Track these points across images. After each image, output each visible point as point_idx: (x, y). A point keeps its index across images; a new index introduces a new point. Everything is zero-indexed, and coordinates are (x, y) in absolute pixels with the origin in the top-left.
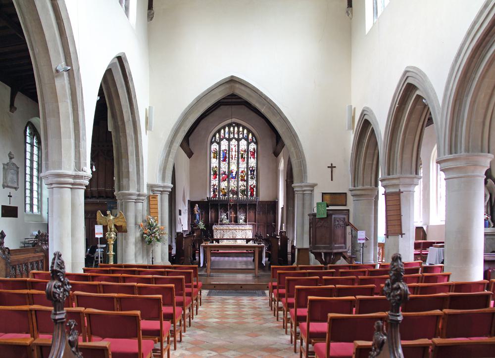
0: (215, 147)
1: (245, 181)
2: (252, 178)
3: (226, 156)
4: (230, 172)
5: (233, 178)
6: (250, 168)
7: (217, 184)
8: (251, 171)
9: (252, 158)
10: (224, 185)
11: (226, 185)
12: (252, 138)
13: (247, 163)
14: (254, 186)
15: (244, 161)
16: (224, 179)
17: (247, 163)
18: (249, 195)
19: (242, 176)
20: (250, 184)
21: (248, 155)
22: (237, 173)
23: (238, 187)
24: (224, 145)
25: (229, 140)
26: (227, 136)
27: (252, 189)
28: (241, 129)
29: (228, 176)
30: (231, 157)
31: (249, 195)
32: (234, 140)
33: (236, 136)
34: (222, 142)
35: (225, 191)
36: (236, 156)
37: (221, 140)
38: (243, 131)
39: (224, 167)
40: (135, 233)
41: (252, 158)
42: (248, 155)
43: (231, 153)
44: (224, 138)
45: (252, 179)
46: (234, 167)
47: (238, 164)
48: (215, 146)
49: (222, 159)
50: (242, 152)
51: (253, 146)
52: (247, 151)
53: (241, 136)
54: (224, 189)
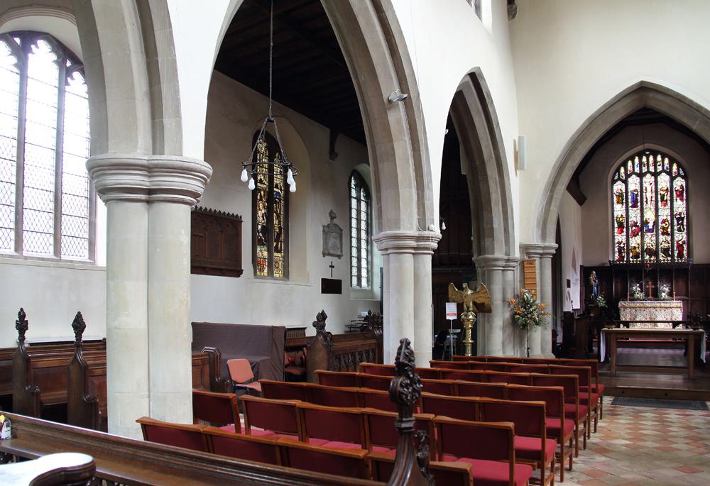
0: (619, 187)
1: (668, 234)
2: (679, 230)
6: (676, 215)
10: (635, 242)
11: (639, 242)
14: (684, 243)
16: (636, 233)
20: (676, 239)
22: (656, 223)
24: (634, 183)
25: (641, 175)
26: (637, 170)
27: (680, 247)
28: (659, 158)
29: (642, 228)
30: (645, 200)
33: (652, 169)
34: (630, 180)
37: (628, 176)
38: (663, 161)
39: (634, 215)
44: (634, 173)
45: (681, 231)
46: (650, 216)
47: (657, 209)
48: (619, 187)
49: (630, 205)
51: (679, 183)
53: (659, 169)
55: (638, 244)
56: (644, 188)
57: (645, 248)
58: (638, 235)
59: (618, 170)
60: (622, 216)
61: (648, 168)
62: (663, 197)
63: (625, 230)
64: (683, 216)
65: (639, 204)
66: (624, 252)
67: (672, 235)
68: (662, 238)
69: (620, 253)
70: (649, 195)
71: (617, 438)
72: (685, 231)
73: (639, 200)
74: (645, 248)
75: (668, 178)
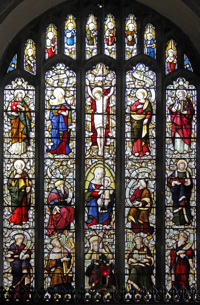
0: (20, 94)
1: (148, 230)
2: (179, 220)
3: (67, 133)
4: (85, 195)
5: (96, 220)
6: (172, 178)
7: (29, 245)
8: (176, 192)
9: (178, 142)
10: (58, 247)
11: (70, 247)
12: (179, 57)
13: (160, 160)
14: (190, 254)
15: (143, 151)
16: (62, 224)
17: (160, 160)
18: (169, 287)
19: (137, 213)
20: (170, 243)
21: (160, 127)
22: (117, 197)
23: (119, 254)
24: (59, 90)
25: (80, 66)
26: (70, 50)
27: (180, 265)
28: (131, 25)
29: (79, 210)
30: (88, 134)
31: (169, 287)
32: (99, 69)
33: (110, 50)
34: (51, 78)
35: (66, 271)
36: (113, 133)
37: (45, 64)
38: (141, 32)
39: (59, 176)
40: (25, 254)
41: (178, 142)
42: (160, 127)
43: (88, 118)
44: (60, 58)
45: (183, 222)
46: (98, 175)
47: (120, 160)
48: (18, 92)
49: (49, 145)
50: (136, 117)
51: (180, 92)
52: (159, 109)
53: (132, 51)
54: (59, 263)
55: (69, 255)
56: (88, 102)
57: (88, 264)
58: (68, 228)
59: (17, 48)
60: (24, 175)
61: (101, 48)
62: (137, 135)
63: (31, 213)
64: (188, 182)
65: (73, 144)
66: (29, 274)
67: (160, 232)
68: (132, 240)
69: (17, 274)
70: (100, 149)
71: (195, 136)
72: (194, 224)
73: (73, 134)
74: (88, 264)
75: (150, 78)
